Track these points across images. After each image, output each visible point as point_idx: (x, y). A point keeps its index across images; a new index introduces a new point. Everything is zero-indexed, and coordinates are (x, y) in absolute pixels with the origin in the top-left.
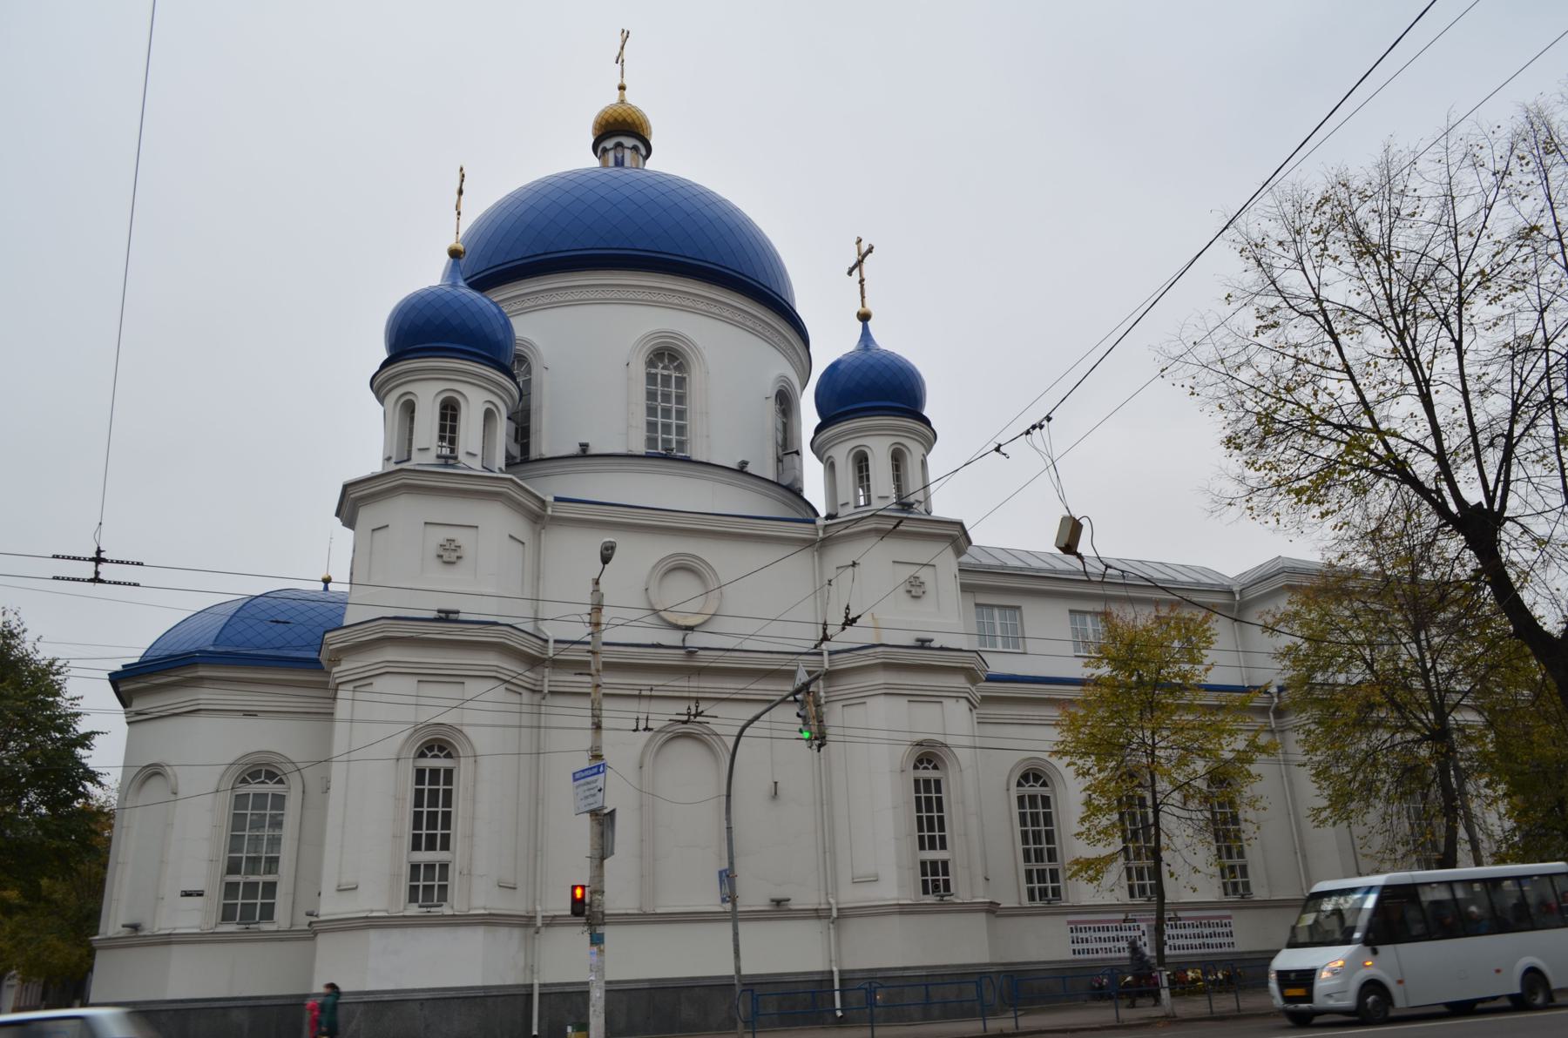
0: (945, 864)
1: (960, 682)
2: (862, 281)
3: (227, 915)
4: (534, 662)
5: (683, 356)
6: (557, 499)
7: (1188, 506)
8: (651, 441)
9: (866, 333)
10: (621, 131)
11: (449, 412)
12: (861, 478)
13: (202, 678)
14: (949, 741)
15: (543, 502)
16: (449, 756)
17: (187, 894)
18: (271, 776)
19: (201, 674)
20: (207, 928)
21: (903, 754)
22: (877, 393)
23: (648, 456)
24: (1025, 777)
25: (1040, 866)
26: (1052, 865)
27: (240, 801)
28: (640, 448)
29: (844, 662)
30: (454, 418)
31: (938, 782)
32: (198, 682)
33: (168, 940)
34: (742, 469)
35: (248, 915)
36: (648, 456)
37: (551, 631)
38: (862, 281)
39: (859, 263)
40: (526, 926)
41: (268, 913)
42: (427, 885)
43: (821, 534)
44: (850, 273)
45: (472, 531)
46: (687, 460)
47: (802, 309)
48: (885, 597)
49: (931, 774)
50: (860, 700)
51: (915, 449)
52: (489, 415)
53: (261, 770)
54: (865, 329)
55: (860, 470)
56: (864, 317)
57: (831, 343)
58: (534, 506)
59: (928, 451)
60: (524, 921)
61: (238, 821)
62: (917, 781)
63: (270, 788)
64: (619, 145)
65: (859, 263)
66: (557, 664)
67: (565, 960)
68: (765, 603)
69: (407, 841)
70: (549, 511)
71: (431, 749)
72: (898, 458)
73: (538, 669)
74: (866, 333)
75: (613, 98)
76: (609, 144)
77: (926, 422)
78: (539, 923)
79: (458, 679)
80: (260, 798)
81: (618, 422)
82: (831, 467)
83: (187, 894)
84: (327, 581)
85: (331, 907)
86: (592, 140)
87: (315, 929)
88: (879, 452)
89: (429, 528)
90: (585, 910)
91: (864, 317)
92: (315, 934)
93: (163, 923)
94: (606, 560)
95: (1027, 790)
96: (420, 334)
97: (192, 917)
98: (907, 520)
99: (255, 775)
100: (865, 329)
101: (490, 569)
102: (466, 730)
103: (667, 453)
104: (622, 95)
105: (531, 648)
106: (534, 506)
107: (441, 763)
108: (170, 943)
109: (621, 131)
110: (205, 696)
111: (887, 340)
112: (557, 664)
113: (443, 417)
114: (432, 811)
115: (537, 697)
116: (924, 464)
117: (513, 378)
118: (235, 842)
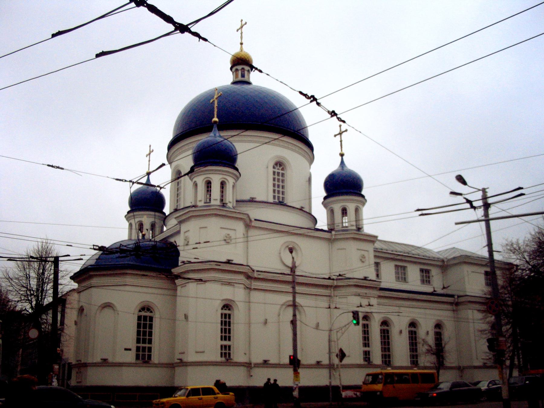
0: (369, 352)
1: (242, 277)
3: (137, 357)
4: (249, 277)
5: (285, 165)
6: (256, 220)
7: (437, 236)
9: (342, 162)
10: (241, 63)
11: (209, 184)
12: (208, 191)
13: (127, 273)
14: (235, 299)
17: (126, 349)
21: (218, 305)
22: (344, 186)
23: (274, 203)
24: (143, 309)
25: (144, 345)
26: (139, 345)
27: (139, 318)
28: (271, 200)
31: (230, 315)
33: (120, 365)
34: (301, 209)
36: (274, 203)
43: (333, 237)
46: (285, 205)
48: (353, 262)
49: (227, 312)
50: (345, 296)
51: (230, 181)
54: (342, 159)
55: (208, 187)
56: (342, 155)
59: (236, 181)
62: (222, 314)
64: (243, 69)
66: (256, 279)
67: (285, 378)
68: (314, 260)
69: (362, 345)
72: (223, 184)
73: (250, 280)
74: (342, 162)
76: (239, 67)
77: (237, 169)
81: (263, 190)
83: (126, 349)
86: (230, 66)
89: (202, 230)
90: (295, 363)
91: (342, 155)
93: (119, 359)
95: (143, 314)
97: (130, 357)
98: (358, 234)
100: (342, 159)
103: (281, 203)
104: (241, 47)
108: (122, 366)
109: (241, 63)
110: (129, 280)
112: (256, 279)
114: (438, 337)
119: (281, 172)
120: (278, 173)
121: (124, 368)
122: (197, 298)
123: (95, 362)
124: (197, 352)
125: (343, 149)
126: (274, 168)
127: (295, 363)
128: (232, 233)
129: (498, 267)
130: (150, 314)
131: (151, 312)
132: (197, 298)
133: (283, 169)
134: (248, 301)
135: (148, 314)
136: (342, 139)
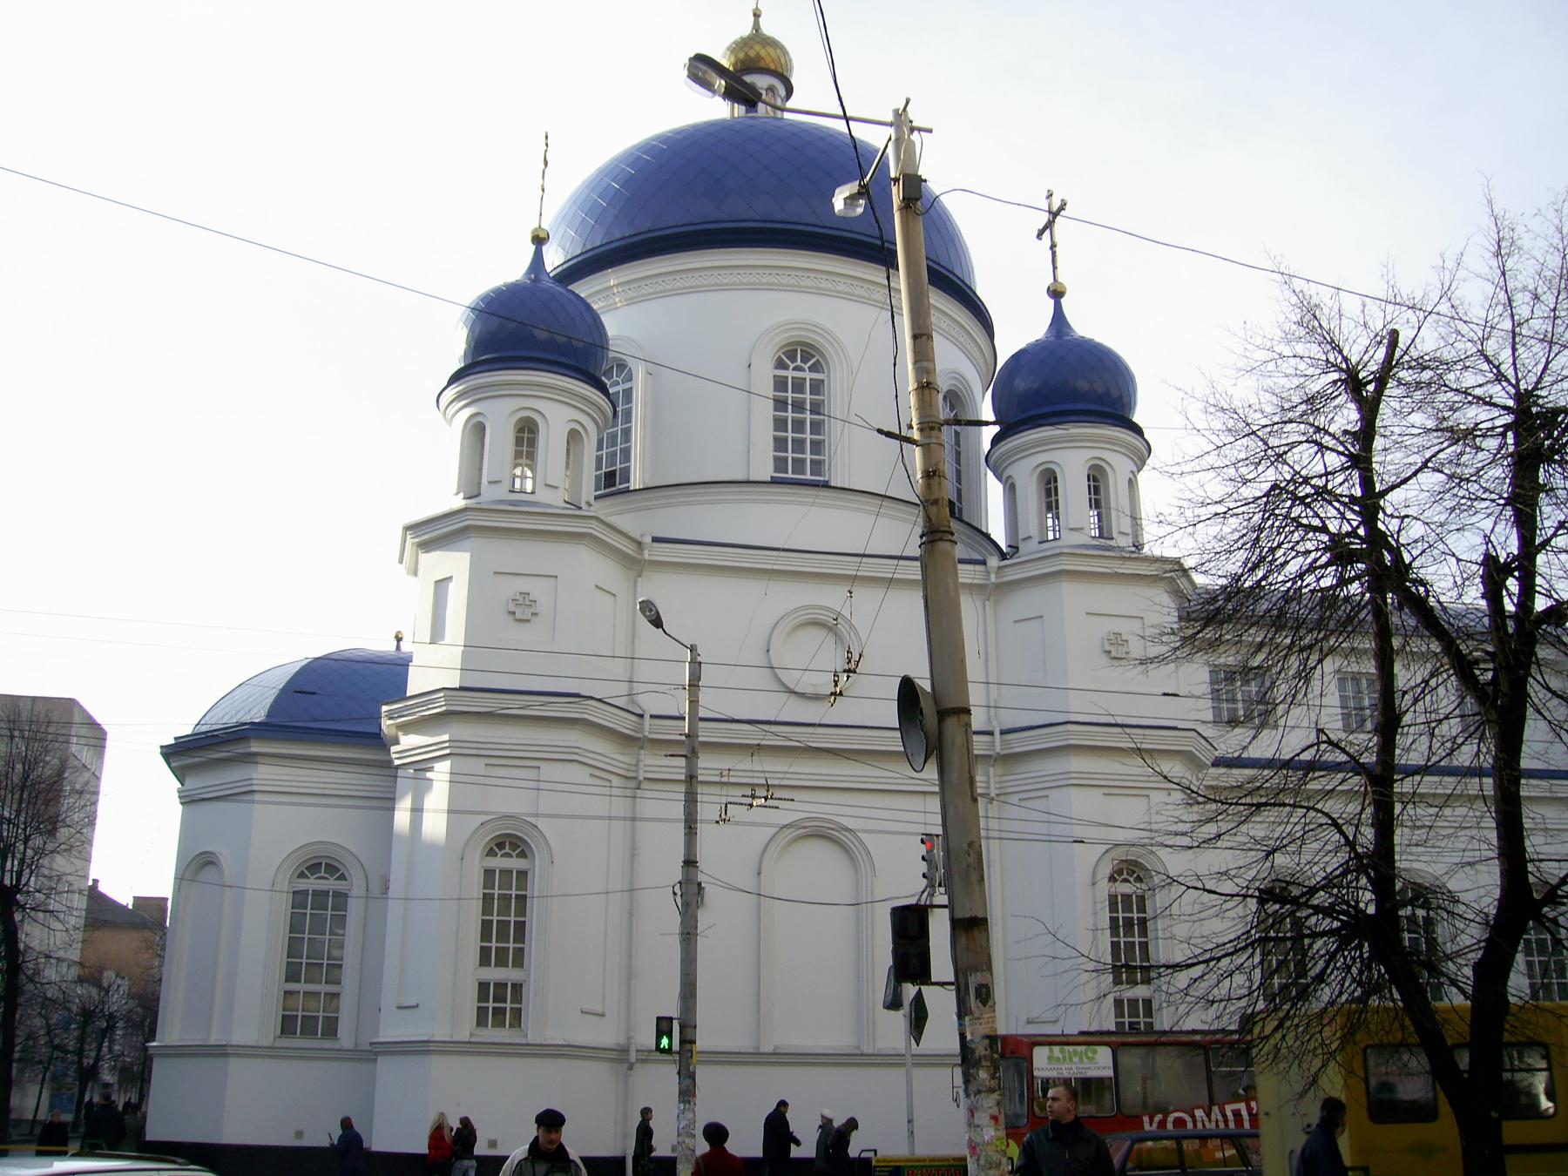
2: (1053, 246)
6: (655, 540)
8: (780, 464)
10: (749, 74)
13: (255, 754)
15: (639, 544)
16: (523, 855)
18: (332, 869)
19: (253, 749)
20: (268, 1040)
23: (774, 482)
27: (299, 898)
29: (1020, 743)
30: (532, 443)
32: (251, 758)
35: (309, 1027)
36: (774, 482)
37: (652, 704)
38: (1053, 246)
39: (1049, 225)
40: (620, 1061)
41: (331, 1029)
42: (500, 1004)
44: (1040, 234)
45: (552, 580)
47: (984, 290)
51: (1119, 465)
52: (574, 436)
53: (320, 864)
54: (1058, 310)
55: (1048, 493)
56: (1056, 294)
57: (1018, 327)
58: (629, 549)
60: (613, 1055)
61: (296, 926)
63: (331, 884)
65: (1049, 225)
69: (474, 955)
70: (646, 555)
71: (501, 846)
72: (1096, 482)
75: (746, 30)
77: (1138, 430)
78: (633, 1058)
79: (531, 760)
80: (320, 895)
82: (1010, 489)
84: (399, 639)
85: (392, 1030)
87: (373, 1052)
88: (1073, 467)
90: (678, 1038)
91: (1056, 294)
92: (377, 1054)
94: (657, 622)
95: (311, 884)
96: (529, 336)
99: (314, 868)
100: (1058, 310)
101: (584, 621)
102: (542, 824)
105: (624, 724)
106: (629, 549)
107: (515, 863)
110: (263, 774)
111: (1085, 324)
113: (519, 441)
114: (505, 925)
115: (632, 784)
116: (1132, 484)
117: (603, 389)
118: (293, 948)
119: (808, 375)
120: (799, 386)
121: (435, 1060)
122: (610, 818)
123: (212, 1041)
124: (400, 1008)
125: (1059, 270)
126: (780, 365)
127: (678, 1038)
128: (536, 588)
129: (970, 586)
130: (340, 886)
131: (342, 877)
132: (610, 818)
133: (815, 368)
134: (628, 815)
135: (331, 884)
136: (1057, 239)
